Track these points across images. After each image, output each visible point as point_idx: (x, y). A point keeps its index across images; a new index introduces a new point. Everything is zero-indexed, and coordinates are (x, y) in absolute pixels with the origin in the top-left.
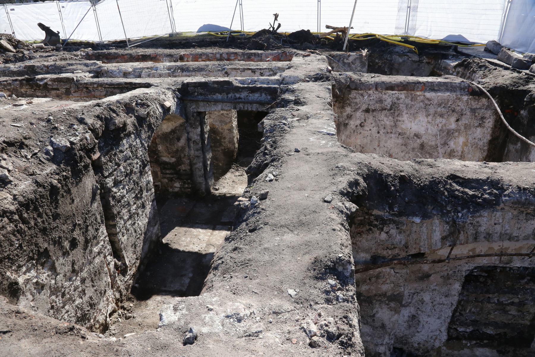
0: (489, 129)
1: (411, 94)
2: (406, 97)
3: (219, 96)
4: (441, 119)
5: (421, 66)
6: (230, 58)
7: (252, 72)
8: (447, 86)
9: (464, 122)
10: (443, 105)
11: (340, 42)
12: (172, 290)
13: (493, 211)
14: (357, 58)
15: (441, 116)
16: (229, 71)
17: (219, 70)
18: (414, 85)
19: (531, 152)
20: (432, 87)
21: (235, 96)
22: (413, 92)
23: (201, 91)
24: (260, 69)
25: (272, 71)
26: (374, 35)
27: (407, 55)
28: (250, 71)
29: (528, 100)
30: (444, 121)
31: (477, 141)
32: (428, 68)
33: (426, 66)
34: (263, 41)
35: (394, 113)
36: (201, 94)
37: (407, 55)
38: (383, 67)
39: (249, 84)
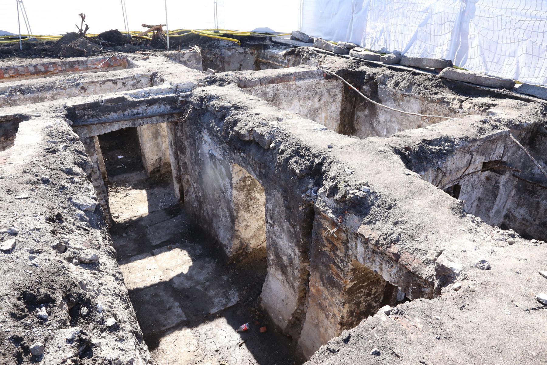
0: (340, 103)
1: (287, 85)
2: (283, 88)
3: (114, 115)
4: (309, 101)
5: (246, 56)
6: (49, 69)
7: (113, 83)
8: (309, 74)
9: (324, 101)
10: (309, 90)
11: (159, 40)
12: (174, 325)
13: (452, 156)
14: (192, 55)
15: (309, 99)
16: (86, 86)
17: (72, 86)
18: (288, 76)
19: (379, 115)
20: (300, 77)
21: (133, 112)
22: (287, 83)
23: (92, 113)
24: (122, 79)
25: (135, 79)
26: (190, 31)
27: (234, 48)
28: (111, 83)
29: (368, 78)
30: (311, 102)
31: (333, 113)
32: (251, 59)
33: (251, 56)
34: (78, 46)
35: (276, 102)
36: (92, 116)
37: (234, 48)
38: (215, 61)
39: (143, 97)
